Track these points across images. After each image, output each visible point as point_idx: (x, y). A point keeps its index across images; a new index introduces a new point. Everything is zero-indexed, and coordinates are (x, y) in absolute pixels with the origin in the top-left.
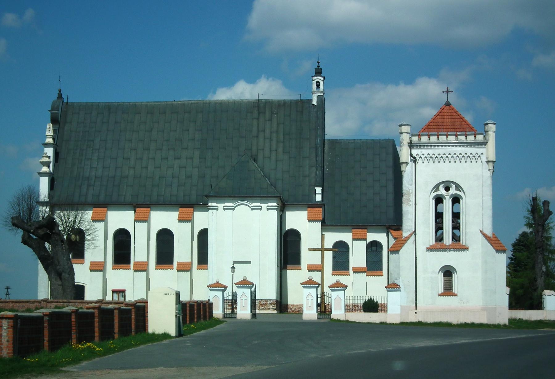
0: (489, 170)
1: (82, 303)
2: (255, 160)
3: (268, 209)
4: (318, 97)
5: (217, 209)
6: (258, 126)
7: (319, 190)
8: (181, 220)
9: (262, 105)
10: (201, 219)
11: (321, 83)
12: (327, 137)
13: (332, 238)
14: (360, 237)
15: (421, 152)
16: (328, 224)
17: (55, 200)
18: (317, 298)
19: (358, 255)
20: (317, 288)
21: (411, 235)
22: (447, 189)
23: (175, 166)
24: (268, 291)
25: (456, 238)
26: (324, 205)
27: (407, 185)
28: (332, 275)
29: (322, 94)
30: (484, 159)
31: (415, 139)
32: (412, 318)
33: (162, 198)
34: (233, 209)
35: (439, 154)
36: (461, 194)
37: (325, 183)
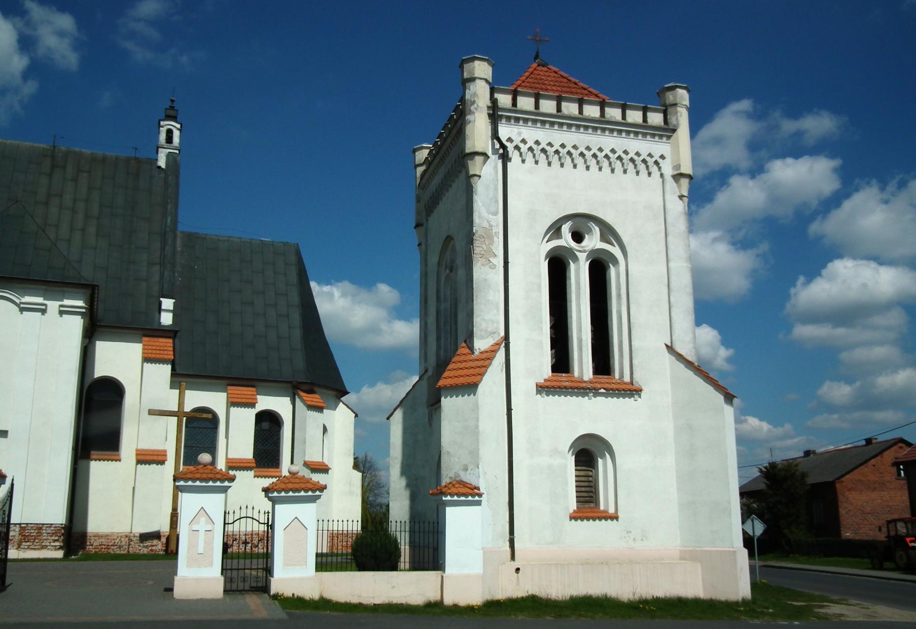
0: (681, 197)
3: (61, 313)
4: (169, 155)
11: (176, 135)
15: (520, 134)
19: (237, 437)
21: (498, 344)
22: (578, 237)
25: (603, 361)
27: (484, 213)
30: (668, 169)
31: (504, 100)
32: (510, 587)
35: (563, 146)
36: (616, 251)
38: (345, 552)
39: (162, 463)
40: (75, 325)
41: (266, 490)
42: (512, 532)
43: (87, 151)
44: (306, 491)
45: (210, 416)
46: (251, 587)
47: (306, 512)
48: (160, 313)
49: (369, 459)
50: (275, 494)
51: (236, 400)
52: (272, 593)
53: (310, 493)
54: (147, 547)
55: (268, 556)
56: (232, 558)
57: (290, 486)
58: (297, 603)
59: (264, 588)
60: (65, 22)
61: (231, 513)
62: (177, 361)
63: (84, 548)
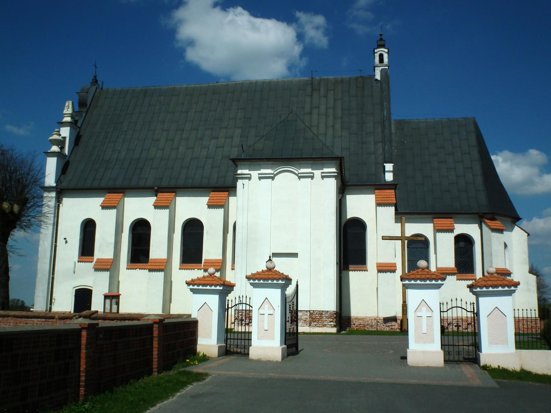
1: (28, 317)
3: (323, 177)
5: (249, 179)
7: (389, 167)
8: (211, 206)
11: (386, 56)
14: (445, 228)
17: (64, 185)
19: (443, 253)
23: (211, 147)
29: (387, 68)
34: (273, 178)
38: (530, 331)
39: (394, 271)
40: (332, 184)
41: (469, 286)
43: (331, 77)
44: (503, 286)
45: (423, 239)
46: (464, 359)
47: (504, 303)
48: (384, 174)
49: (534, 267)
50: (478, 289)
51: (440, 228)
52: (482, 364)
53: (506, 288)
54: (388, 326)
55: (476, 334)
56: (448, 335)
57: (490, 283)
58: (500, 373)
59: (475, 360)
60: (320, 20)
61: (445, 303)
62: (398, 205)
63: (350, 326)
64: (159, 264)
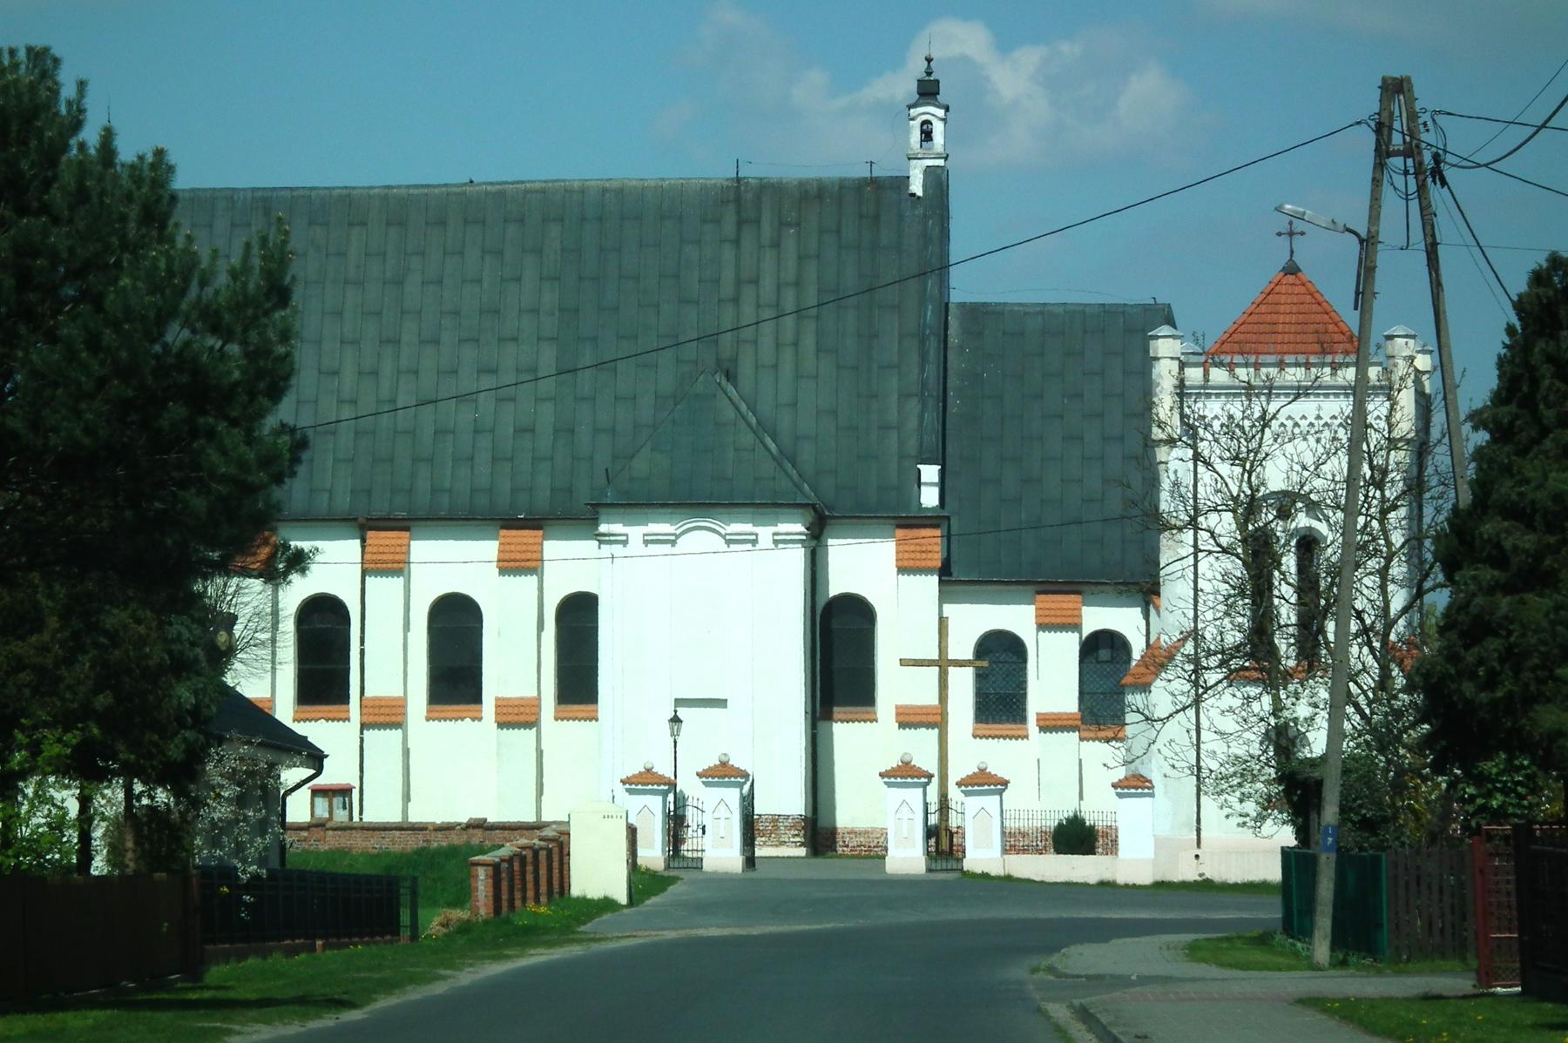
2: (730, 376)
4: (928, 171)
5: (625, 543)
6: (737, 266)
7: (930, 473)
8: (510, 566)
9: (749, 196)
10: (569, 563)
11: (938, 129)
12: (956, 297)
13: (975, 620)
14: (1058, 620)
16: (956, 579)
18: (926, 813)
19: (1054, 677)
20: (925, 786)
24: (784, 795)
26: (948, 518)
28: (975, 736)
31: (1194, 375)
32: (1186, 871)
33: (445, 500)
34: (673, 543)
37: (949, 449)
42: (1199, 821)
64: (387, 711)
